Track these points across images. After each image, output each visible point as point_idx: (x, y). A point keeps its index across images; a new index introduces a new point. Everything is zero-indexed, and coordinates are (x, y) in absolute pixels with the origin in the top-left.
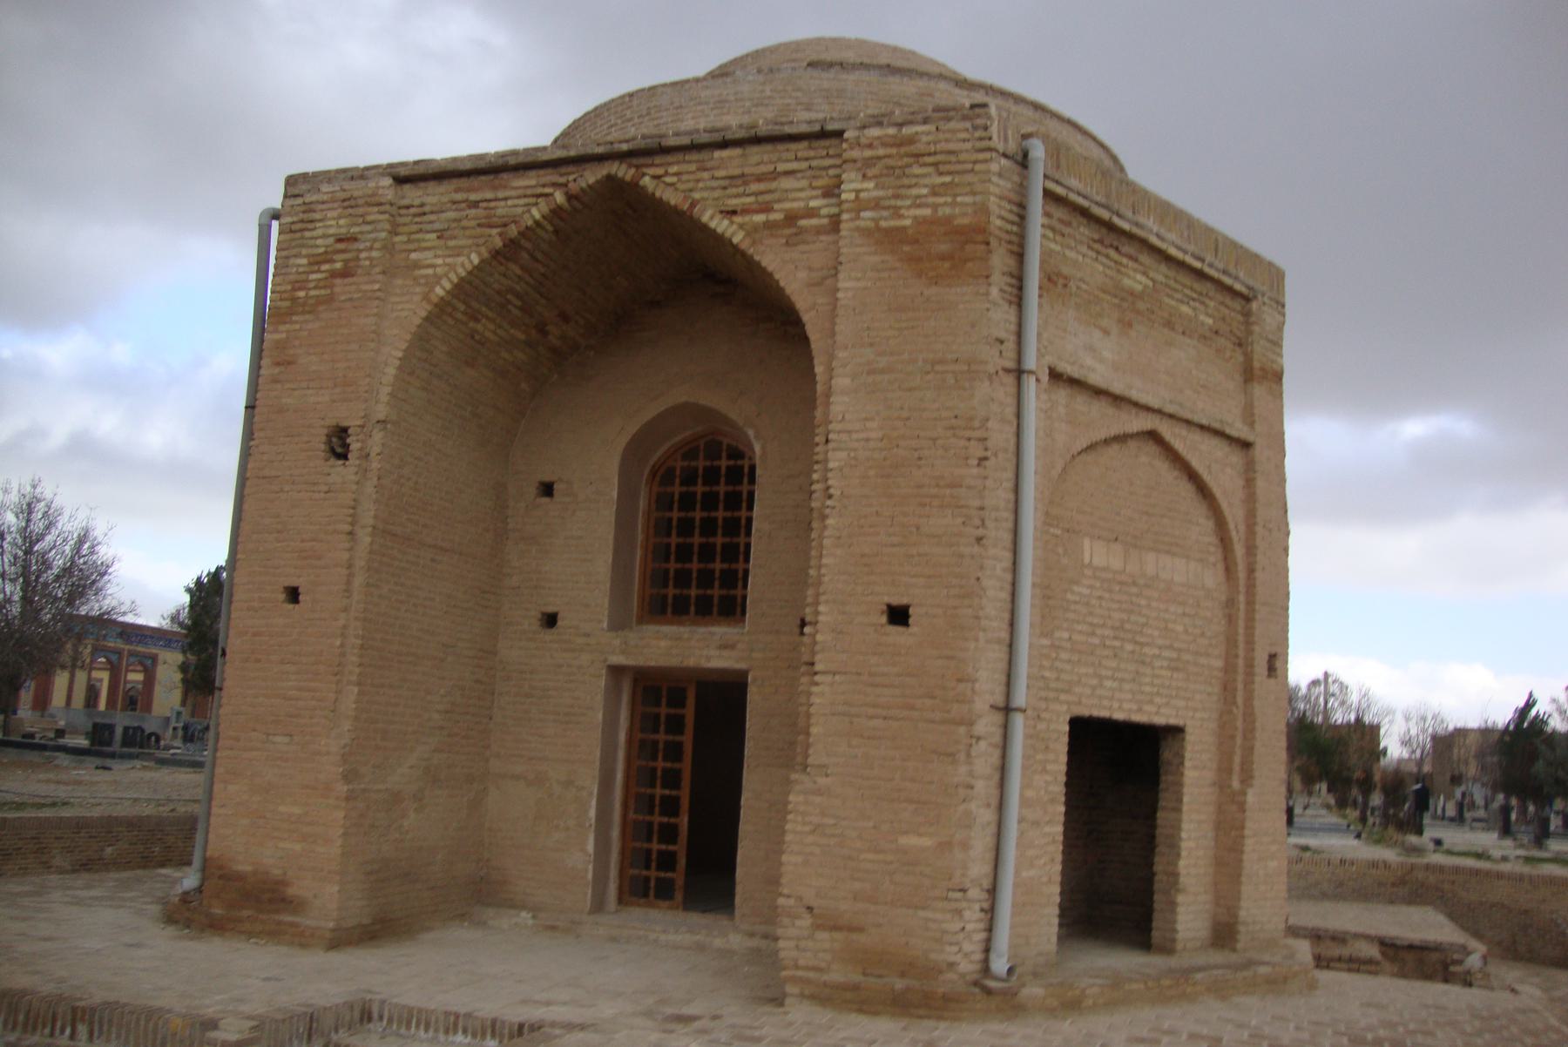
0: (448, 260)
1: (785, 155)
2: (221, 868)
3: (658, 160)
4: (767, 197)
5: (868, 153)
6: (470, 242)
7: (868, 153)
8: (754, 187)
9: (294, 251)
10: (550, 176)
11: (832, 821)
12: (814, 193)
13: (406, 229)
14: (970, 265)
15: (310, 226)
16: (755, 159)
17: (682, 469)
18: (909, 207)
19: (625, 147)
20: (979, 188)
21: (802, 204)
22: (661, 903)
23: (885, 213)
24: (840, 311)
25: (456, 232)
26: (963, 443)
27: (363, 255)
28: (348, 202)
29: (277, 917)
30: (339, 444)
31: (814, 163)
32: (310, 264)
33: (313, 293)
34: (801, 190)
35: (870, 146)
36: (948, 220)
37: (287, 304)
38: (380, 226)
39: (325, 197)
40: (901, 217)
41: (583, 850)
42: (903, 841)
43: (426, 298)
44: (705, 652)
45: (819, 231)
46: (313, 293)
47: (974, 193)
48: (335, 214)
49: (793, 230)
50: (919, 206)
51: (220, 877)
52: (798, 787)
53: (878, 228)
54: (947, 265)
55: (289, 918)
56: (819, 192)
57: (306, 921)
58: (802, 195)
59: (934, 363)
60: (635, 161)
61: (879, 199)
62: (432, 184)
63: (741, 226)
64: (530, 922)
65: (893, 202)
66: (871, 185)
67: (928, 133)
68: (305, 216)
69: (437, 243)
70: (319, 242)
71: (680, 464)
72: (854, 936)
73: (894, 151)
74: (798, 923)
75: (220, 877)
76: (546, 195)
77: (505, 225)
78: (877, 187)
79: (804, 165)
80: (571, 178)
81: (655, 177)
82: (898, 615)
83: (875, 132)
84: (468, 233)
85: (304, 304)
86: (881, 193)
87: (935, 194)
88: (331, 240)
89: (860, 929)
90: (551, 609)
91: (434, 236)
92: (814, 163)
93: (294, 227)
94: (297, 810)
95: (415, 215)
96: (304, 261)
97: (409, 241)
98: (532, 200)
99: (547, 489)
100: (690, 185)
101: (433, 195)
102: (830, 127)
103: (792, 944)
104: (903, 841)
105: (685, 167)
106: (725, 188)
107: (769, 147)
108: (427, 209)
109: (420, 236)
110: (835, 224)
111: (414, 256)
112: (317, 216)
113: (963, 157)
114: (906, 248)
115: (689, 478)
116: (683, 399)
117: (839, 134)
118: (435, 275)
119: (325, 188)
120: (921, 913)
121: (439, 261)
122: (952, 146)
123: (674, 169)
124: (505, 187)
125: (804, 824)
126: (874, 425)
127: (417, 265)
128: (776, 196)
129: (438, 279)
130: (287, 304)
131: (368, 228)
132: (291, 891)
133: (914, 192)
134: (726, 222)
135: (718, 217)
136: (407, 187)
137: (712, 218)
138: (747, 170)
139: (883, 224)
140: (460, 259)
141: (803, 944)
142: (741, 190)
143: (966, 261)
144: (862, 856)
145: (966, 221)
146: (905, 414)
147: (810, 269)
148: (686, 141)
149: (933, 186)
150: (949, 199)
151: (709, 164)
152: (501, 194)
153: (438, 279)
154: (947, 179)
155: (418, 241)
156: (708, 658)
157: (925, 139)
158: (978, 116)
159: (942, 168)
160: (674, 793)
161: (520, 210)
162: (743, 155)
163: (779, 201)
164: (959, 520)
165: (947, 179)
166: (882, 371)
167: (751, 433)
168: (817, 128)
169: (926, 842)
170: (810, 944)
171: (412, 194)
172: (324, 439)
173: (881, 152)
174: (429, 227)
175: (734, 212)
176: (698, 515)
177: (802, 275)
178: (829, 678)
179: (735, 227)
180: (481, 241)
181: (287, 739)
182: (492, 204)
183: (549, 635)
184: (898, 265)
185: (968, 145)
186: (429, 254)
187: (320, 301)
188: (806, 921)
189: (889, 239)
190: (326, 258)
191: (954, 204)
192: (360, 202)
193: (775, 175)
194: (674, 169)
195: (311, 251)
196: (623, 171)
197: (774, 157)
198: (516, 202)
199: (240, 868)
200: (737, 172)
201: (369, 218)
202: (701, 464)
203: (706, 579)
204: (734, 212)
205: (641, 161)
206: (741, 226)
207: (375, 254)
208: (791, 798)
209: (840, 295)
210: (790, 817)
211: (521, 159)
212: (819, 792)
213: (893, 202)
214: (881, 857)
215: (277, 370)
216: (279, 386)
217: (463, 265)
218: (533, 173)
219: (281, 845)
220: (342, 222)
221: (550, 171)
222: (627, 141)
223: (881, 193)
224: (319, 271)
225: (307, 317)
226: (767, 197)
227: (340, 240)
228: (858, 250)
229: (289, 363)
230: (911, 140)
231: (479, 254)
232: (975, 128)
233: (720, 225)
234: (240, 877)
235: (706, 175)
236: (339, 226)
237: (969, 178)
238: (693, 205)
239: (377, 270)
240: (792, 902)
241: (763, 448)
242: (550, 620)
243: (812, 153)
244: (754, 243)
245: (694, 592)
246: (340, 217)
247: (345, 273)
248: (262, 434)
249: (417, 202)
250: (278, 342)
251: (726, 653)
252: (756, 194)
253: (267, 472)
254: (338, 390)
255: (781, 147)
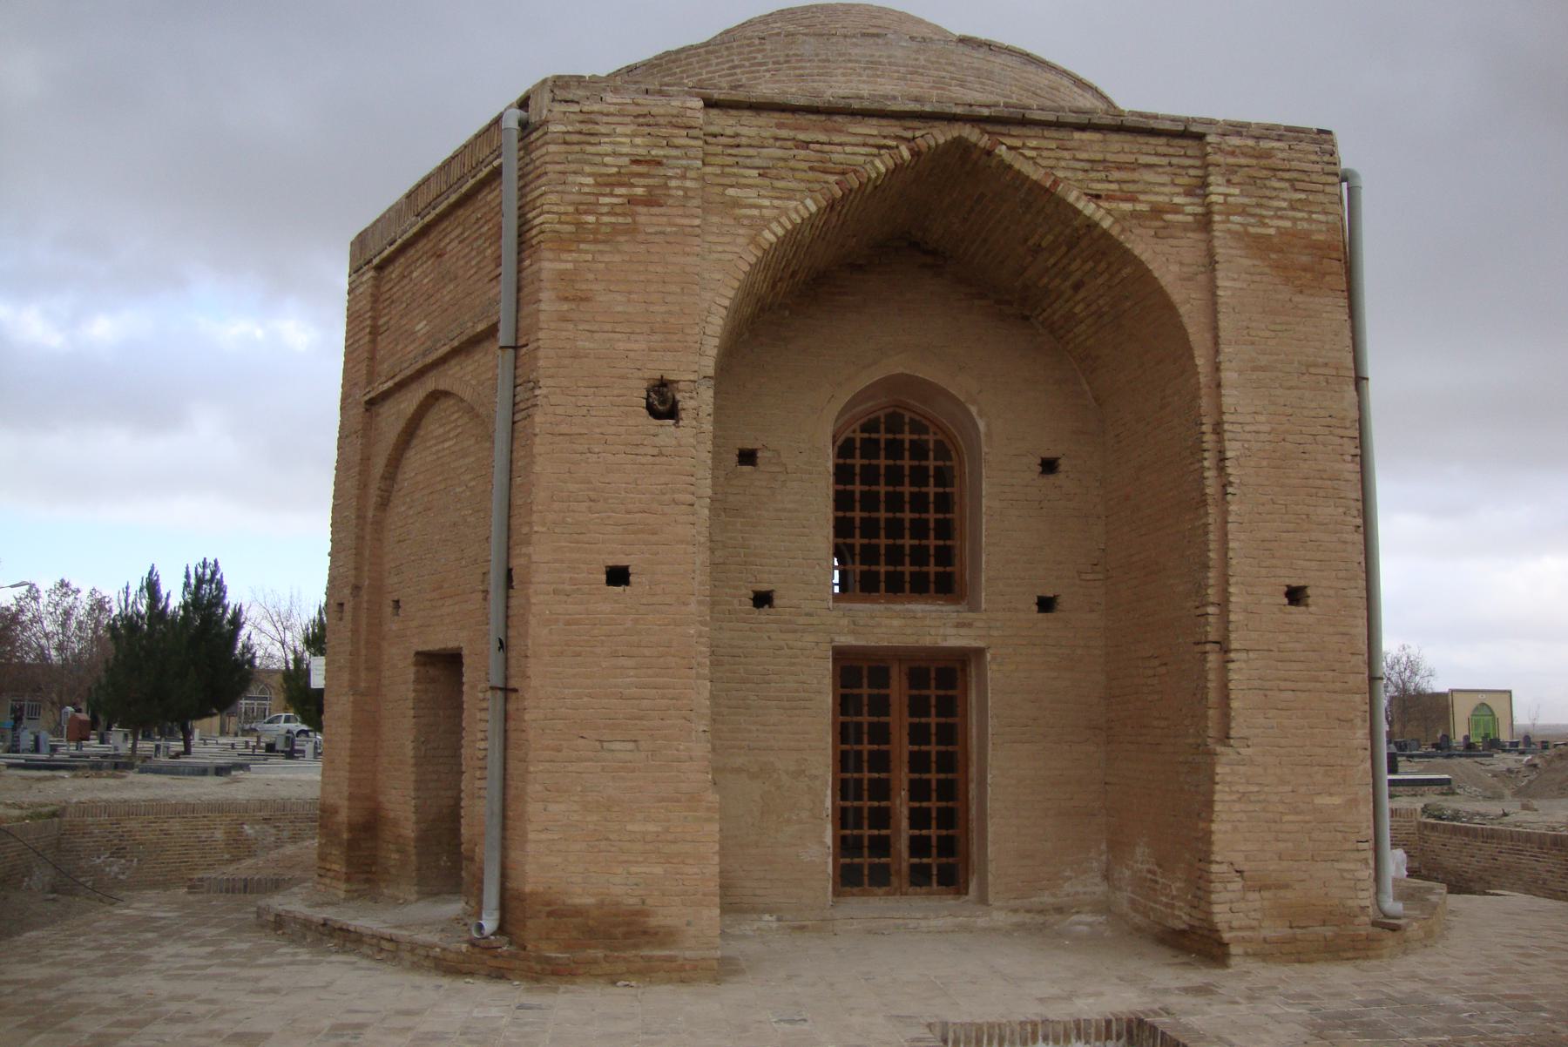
0: (776, 203)
1: (1145, 149)
2: (548, 904)
3: (1015, 131)
4: (1132, 187)
5: (1231, 160)
6: (802, 186)
7: (1231, 160)
8: (1116, 175)
9: (573, 167)
10: (894, 128)
11: (1256, 789)
12: (1178, 190)
13: (718, 160)
14: (1328, 278)
15: (592, 139)
16: (1116, 147)
17: (927, 441)
18: (1271, 217)
19: (986, 112)
20: (1330, 208)
21: (1167, 199)
22: (875, 889)
23: (1252, 220)
24: (1222, 308)
25: (783, 173)
26: (1339, 441)
27: (673, 183)
28: (645, 120)
29: (646, 952)
30: (663, 403)
31: (1175, 161)
32: (597, 184)
33: (605, 219)
34: (1163, 185)
35: (1233, 154)
36: (1307, 234)
37: (571, 228)
38: (691, 153)
39: (612, 109)
40: (1265, 225)
41: (822, 843)
42: (1318, 800)
43: (753, 241)
44: (941, 631)
45: (1185, 227)
46: (605, 219)
47: (1326, 213)
48: (628, 130)
49: (1160, 224)
50: (1281, 218)
51: (550, 914)
52: (1224, 759)
53: (1248, 234)
54: (1309, 276)
55: (657, 953)
56: (1181, 190)
57: (686, 952)
58: (1166, 190)
59: (1308, 366)
60: (989, 128)
61: (1245, 206)
62: (747, 113)
63: (1109, 212)
64: (775, 925)
65: (1258, 211)
66: (1236, 191)
67: (1283, 150)
68: (584, 128)
69: (759, 181)
70: (607, 160)
71: (931, 439)
72: (1282, 893)
73: (1254, 162)
74: (1230, 887)
75: (550, 914)
76: (888, 147)
77: (843, 173)
78: (1242, 194)
79: (1164, 161)
80: (918, 134)
81: (1010, 148)
82: (1295, 595)
83: (1235, 141)
84: (799, 175)
85: (596, 232)
86: (1246, 200)
87: (1293, 209)
88: (626, 160)
89: (1286, 886)
90: (764, 587)
91: (755, 172)
92: (1175, 161)
93: (568, 138)
94: (652, 828)
95: (726, 146)
96: (590, 180)
97: (723, 174)
98: (875, 151)
99: (1049, 466)
100: (1052, 163)
101: (751, 127)
102: (1195, 129)
103: (1226, 908)
104: (1318, 800)
105: (1044, 143)
106: (1086, 171)
107: (1129, 137)
108: (744, 141)
109: (735, 170)
110: (1205, 222)
111: (731, 192)
112: (603, 129)
113: (1314, 177)
114: (1273, 256)
115: (919, 450)
116: (900, 370)
117: (1200, 137)
118: (762, 217)
119: (610, 97)
120: (1336, 865)
121: (766, 202)
122: (1305, 166)
123: (1033, 143)
124: (840, 131)
125: (1231, 792)
126: (1261, 418)
127: (736, 203)
128: (1140, 187)
129: (766, 223)
130: (571, 228)
131: (674, 152)
132: (653, 922)
133: (1276, 203)
134: (1092, 206)
135: (1085, 198)
136: (713, 112)
137: (1078, 199)
138: (1109, 157)
139: (1252, 230)
140: (793, 204)
141: (1236, 906)
142: (1103, 175)
143: (1324, 275)
144: (1286, 818)
145: (1321, 237)
146: (1290, 411)
147: (1181, 264)
148: (1051, 117)
149: (1291, 201)
150: (1305, 215)
151: (1069, 144)
152: (836, 139)
153: (766, 223)
154: (1303, 196)
155: (735, 175)
156: (945, 637)
157: (1280, 155)
158: (1326, 142)
159: (1299, 185)
160: (883, 775)
161: (861, 159)
162: (1104, 141)
163: (1145, 193)
164: (1341, 510)
165: (1303, 196)
166: (1263, 369)
167: (973, 410)
168: (1181, 128)
169: (1337, 800)
170: (1243, 905)
171: (722, 122)
172: (644, 394)
173: (1243, 161)
174: (748, 162)
175: (1098, 197)
176: (882, 489)
177: (1174, 268)
178: (1243, 655)
179: (1102, 212)
180: (817, 186)
181: (631, 746)
182: (827, 148)
183: (764, 614)
184: (1267, 270)
185: (1318, 167)
186: (752, 193)
187: (616, 229)
188: (1237, 885)
189: (1259, 245)
190: (620, 179)
191: (1310, 220)
192: (661, 121)
193: (1135, 166)
194: (1033, 143)
195: (595, 169)
196: (971, 134)
197: (1135, 148)
198: (857, 149)
199: (577, 901)
200: (1099, 157)
201: (677, 141)
202: (883, 436)
203: (919, 556)
204: (1098, 197)
205: (998, 129)
206: (1109, 212)
207: (688, 184)
208: (1219, 770)
209: (1220, 293)
210: (1218, 787)
211: (866, 104)
212: (1242, 763)
213: (1258, 211)
214: (1300, 818)
215: (565, 307)
216: (570, 326)
217: (797, 211)
218: (874, 121)
219: (634, 869)
220: (638, 141)
221: (893, 122)
222: (988, 106)
223: (1246, 200)
224: (612, 195)
225: (601, 247)
226: (1132, 187)
227: (636, 162)
228: (1233, 252)
229: (587, 299)
230: (1268, 154)
231: (815, 201)
232: (1324, 153)
233: (1088, 208)
234: (578, 912)
235: (1066, 154)
236: (633, 145)
237: (1321, 198)
238: (1056, 182)
239: (696, 202)
240: (1224, 868)
241: (988, 425)
242: (762, 599)
243: (1171, 151)
244: (1123, 230)
245: (883, 569)
246: (635, 136)
247: (650, 201)
248: (550, 382)
249: (729, 131)
250: (562, 273)
251: (963, 631)
252: (1119, 182)
253: (564, 429)
254: (656, 337)
255: (1141, 139)
